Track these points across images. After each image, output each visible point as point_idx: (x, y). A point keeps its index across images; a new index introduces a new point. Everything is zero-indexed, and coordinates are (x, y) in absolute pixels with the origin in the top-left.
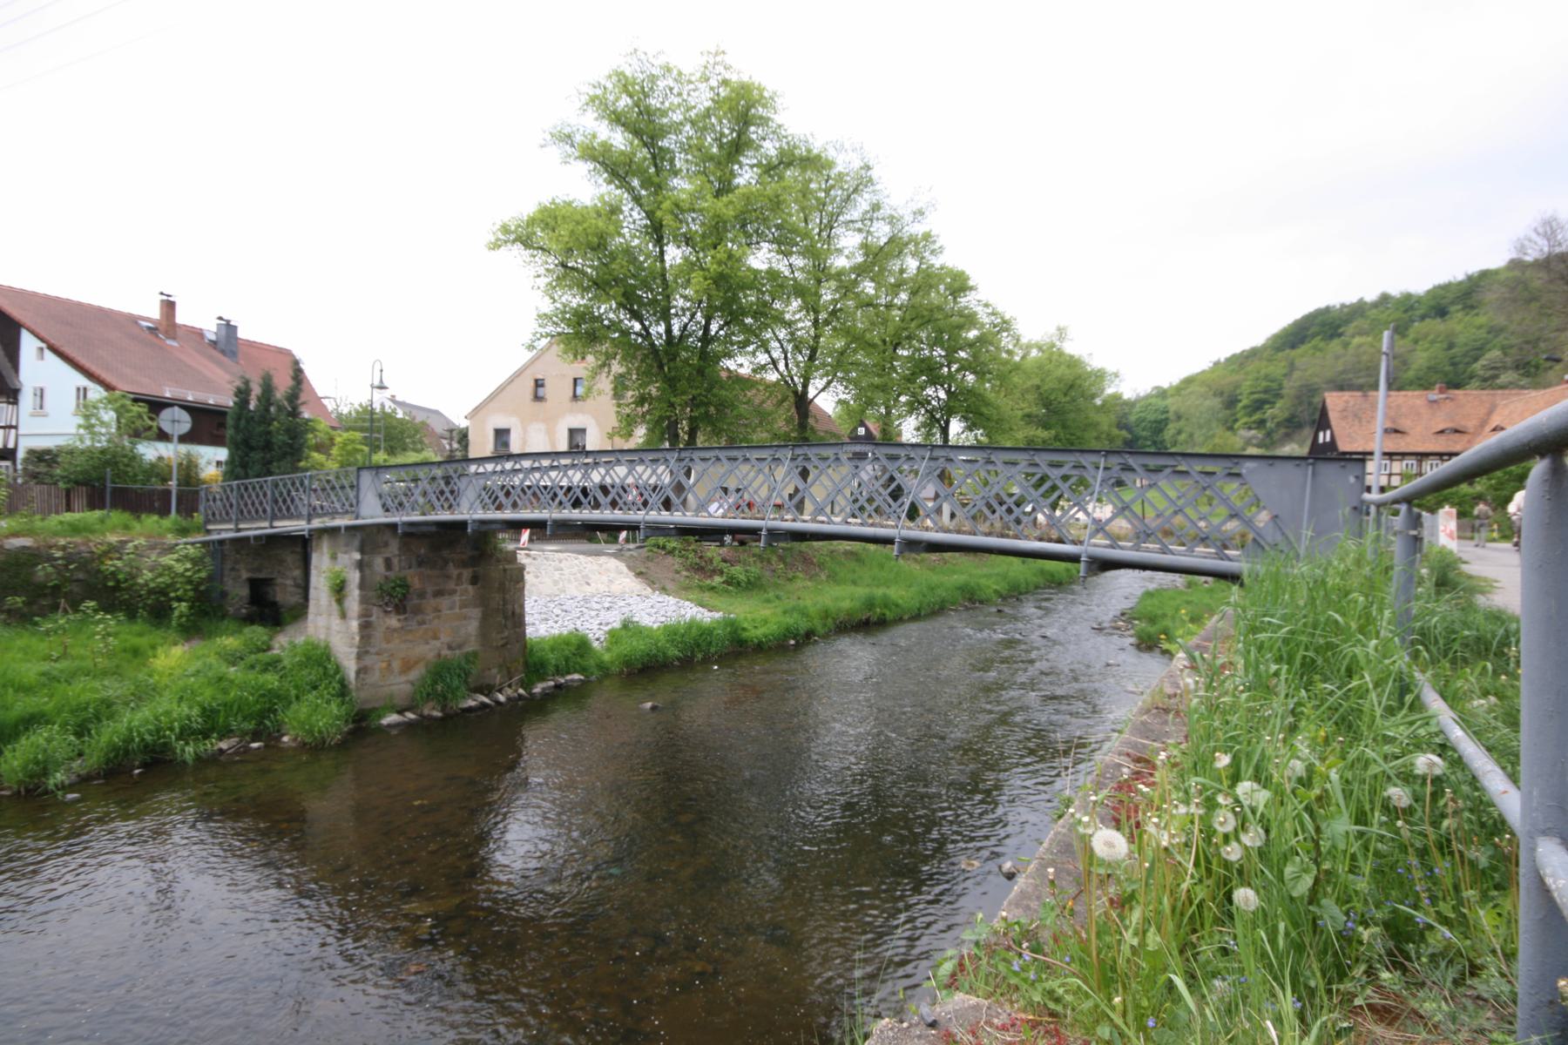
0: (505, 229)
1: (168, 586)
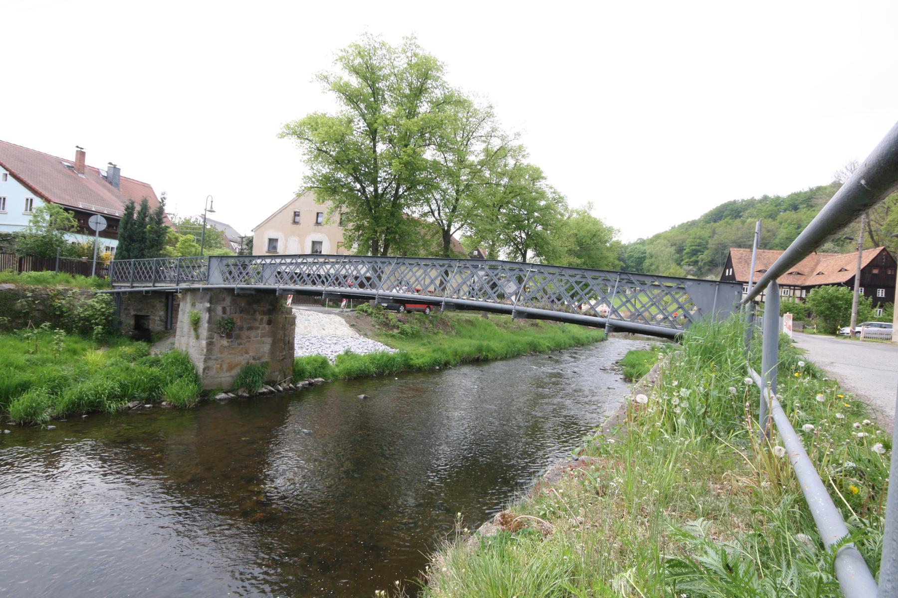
0: (288, 126)
1: (91, 316)
